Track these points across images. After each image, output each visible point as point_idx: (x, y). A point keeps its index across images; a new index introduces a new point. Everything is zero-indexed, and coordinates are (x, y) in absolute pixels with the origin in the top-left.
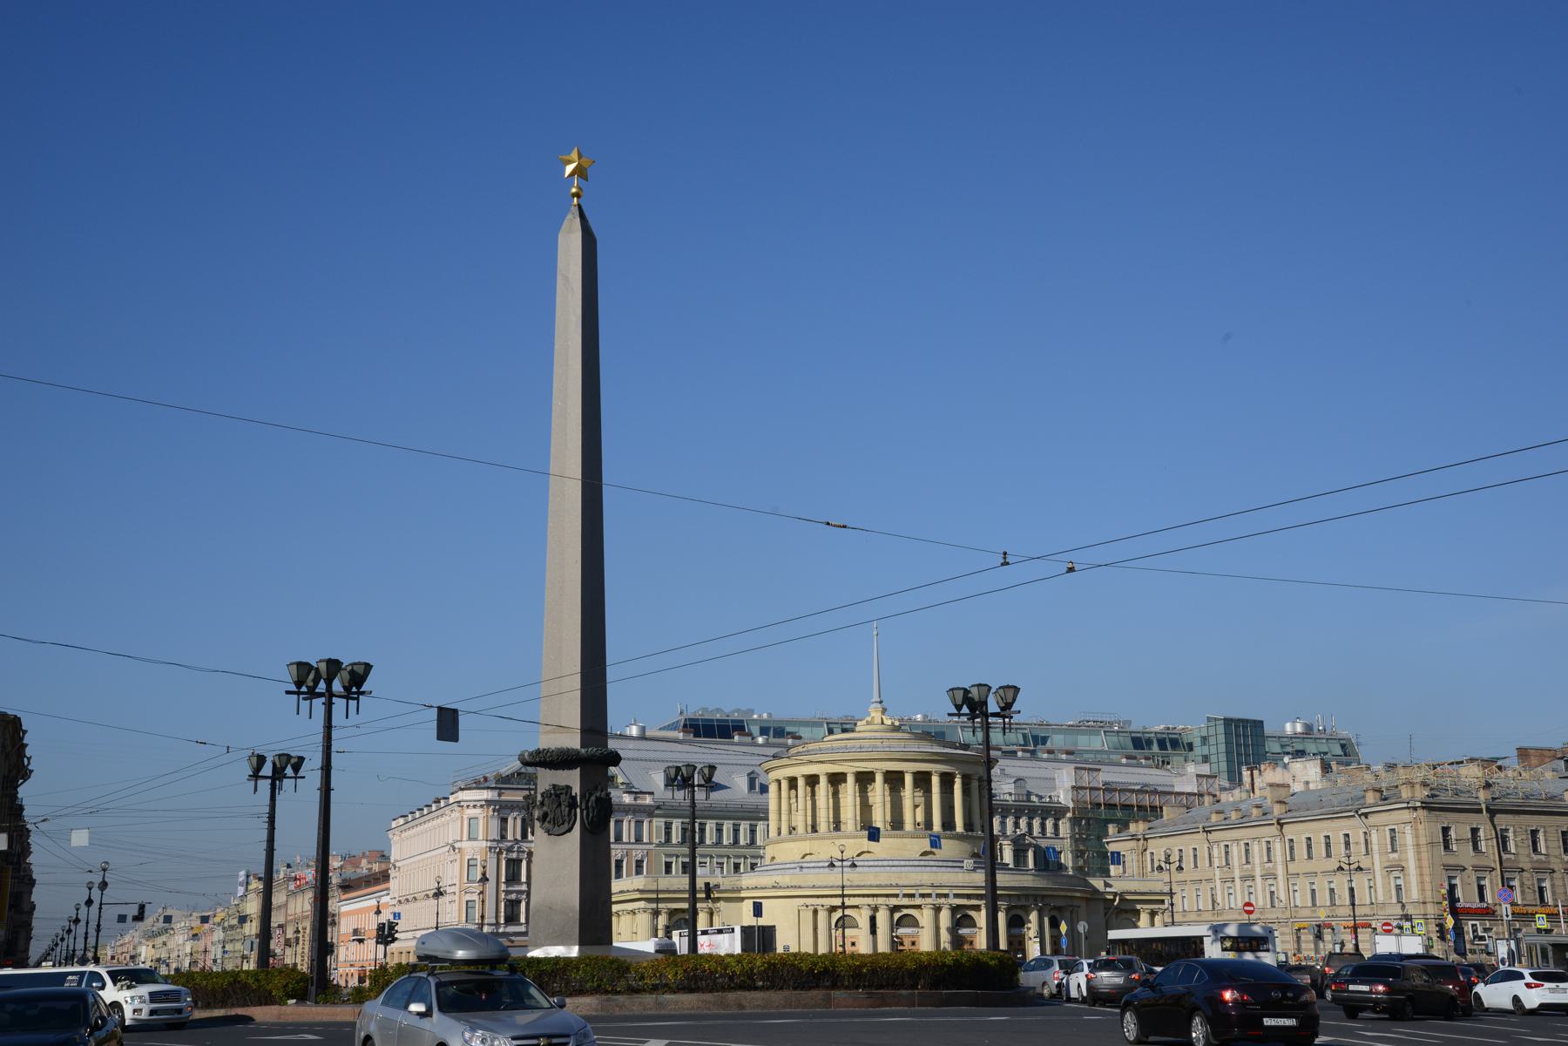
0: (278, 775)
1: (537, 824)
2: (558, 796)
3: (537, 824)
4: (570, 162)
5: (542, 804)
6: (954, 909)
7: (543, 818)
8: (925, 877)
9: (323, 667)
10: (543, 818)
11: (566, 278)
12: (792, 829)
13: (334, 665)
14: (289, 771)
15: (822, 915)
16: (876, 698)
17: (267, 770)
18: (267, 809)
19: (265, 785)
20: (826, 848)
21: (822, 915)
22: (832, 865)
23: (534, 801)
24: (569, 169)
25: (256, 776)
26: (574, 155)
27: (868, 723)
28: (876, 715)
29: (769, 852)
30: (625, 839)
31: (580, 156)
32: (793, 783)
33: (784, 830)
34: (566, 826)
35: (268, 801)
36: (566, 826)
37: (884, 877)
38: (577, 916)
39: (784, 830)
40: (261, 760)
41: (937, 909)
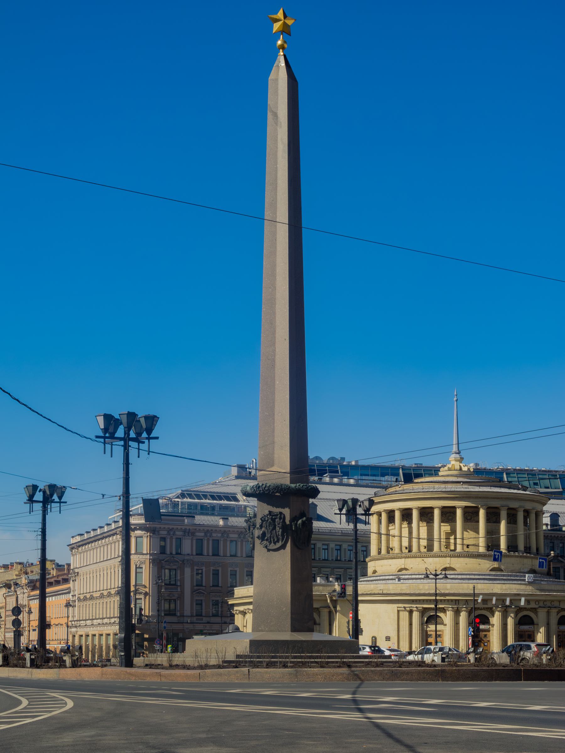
0: (47, 501)
1: (257, 542)
2: (274, 520)
3: (257, 542)
4: (277, 20)
5: (261, 526)
6: (423, 612)
7: (262, 537)
8: (498, 588)
9: (124, 419)
10: (262, 537)
11: (275, 115)
12: (389, 549)
13: (132, 416)
14: (55, 497)
15: (416, 615)
16: (455, 449)
17: (39, 496)
18: (40, 526)
19: (38, 507)
20: (434, 564)
21: (416, 615)
22: (427, 577)
23: (254, 526)
24: (277, 26)
25: (31, 500)
26: (280, 15)
27: (449, 470)
28: (453, 463)
29: (371, 566)
30: (205, 553)
31: (285, 17)
32: (391, 515)
33: (384, 551)
34: (279, 544)
35: (40, 520)
36: (279, 544)
37: (466, 587)
38: (289, 611)
39: (384, 551)
40: (35, 487)
41: (411, 612)
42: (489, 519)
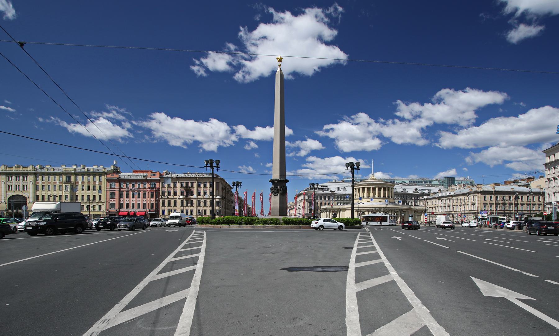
0: (237, 185)
19: (235, 187)
42: (378, 190)
